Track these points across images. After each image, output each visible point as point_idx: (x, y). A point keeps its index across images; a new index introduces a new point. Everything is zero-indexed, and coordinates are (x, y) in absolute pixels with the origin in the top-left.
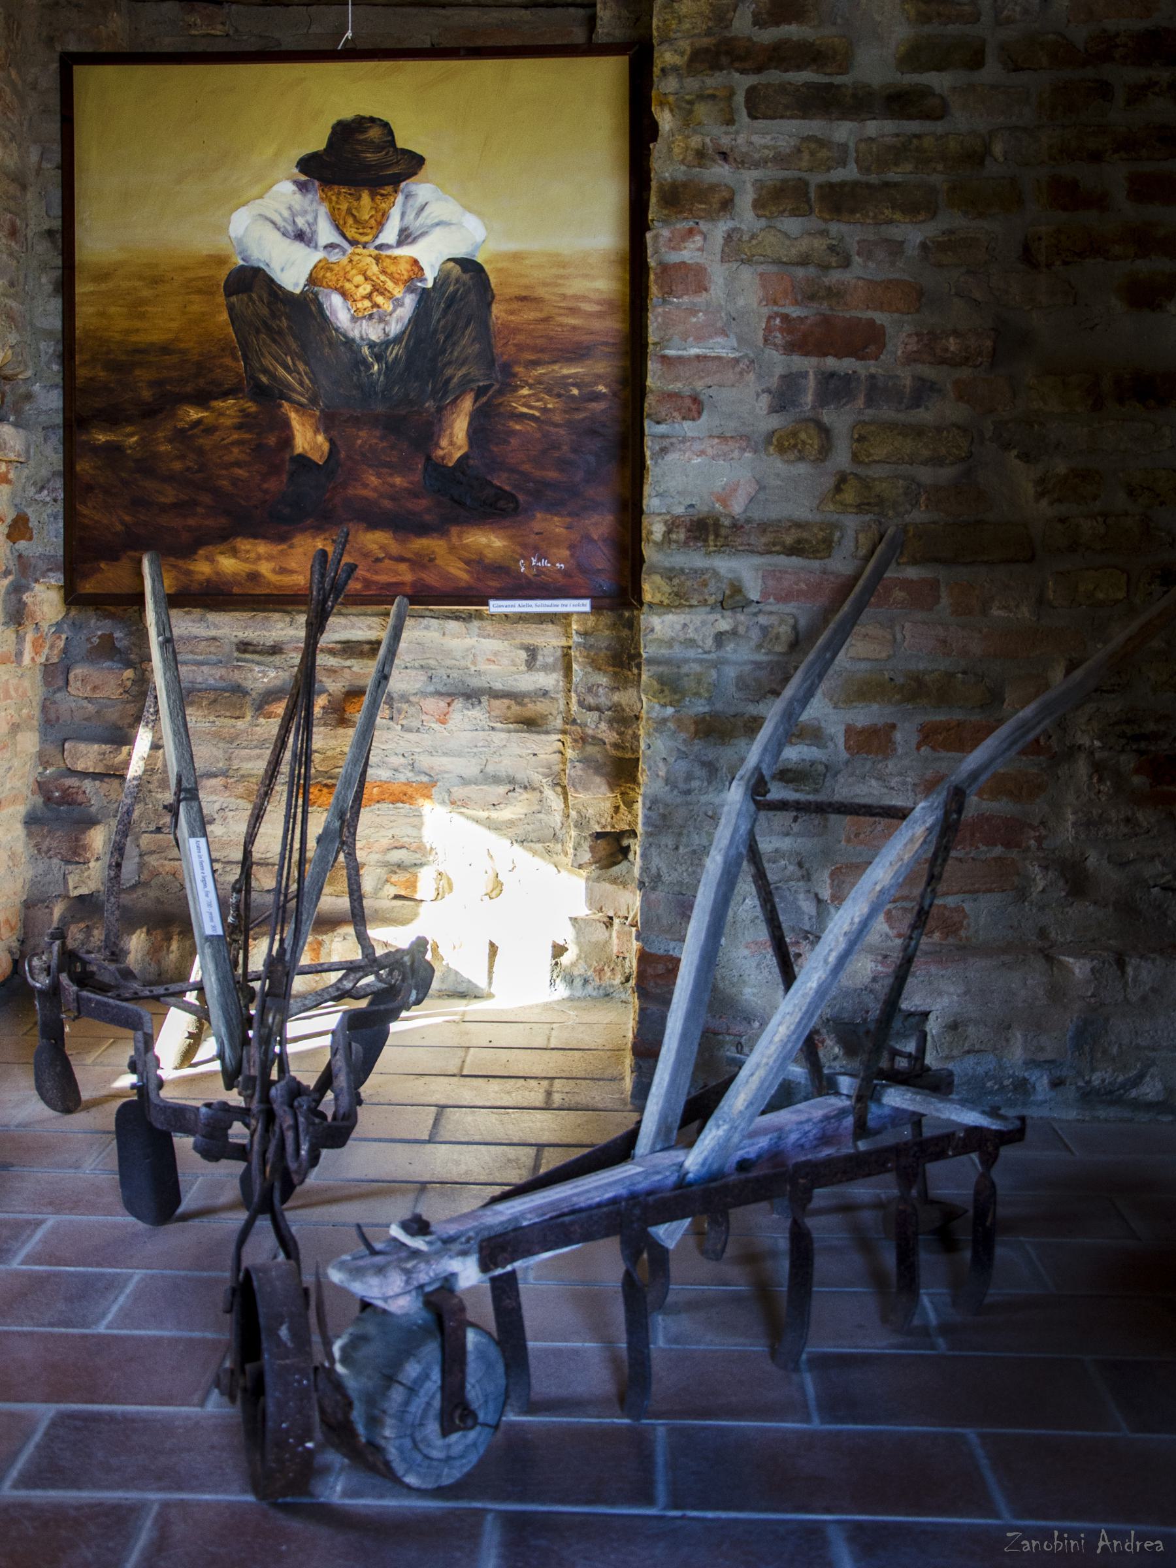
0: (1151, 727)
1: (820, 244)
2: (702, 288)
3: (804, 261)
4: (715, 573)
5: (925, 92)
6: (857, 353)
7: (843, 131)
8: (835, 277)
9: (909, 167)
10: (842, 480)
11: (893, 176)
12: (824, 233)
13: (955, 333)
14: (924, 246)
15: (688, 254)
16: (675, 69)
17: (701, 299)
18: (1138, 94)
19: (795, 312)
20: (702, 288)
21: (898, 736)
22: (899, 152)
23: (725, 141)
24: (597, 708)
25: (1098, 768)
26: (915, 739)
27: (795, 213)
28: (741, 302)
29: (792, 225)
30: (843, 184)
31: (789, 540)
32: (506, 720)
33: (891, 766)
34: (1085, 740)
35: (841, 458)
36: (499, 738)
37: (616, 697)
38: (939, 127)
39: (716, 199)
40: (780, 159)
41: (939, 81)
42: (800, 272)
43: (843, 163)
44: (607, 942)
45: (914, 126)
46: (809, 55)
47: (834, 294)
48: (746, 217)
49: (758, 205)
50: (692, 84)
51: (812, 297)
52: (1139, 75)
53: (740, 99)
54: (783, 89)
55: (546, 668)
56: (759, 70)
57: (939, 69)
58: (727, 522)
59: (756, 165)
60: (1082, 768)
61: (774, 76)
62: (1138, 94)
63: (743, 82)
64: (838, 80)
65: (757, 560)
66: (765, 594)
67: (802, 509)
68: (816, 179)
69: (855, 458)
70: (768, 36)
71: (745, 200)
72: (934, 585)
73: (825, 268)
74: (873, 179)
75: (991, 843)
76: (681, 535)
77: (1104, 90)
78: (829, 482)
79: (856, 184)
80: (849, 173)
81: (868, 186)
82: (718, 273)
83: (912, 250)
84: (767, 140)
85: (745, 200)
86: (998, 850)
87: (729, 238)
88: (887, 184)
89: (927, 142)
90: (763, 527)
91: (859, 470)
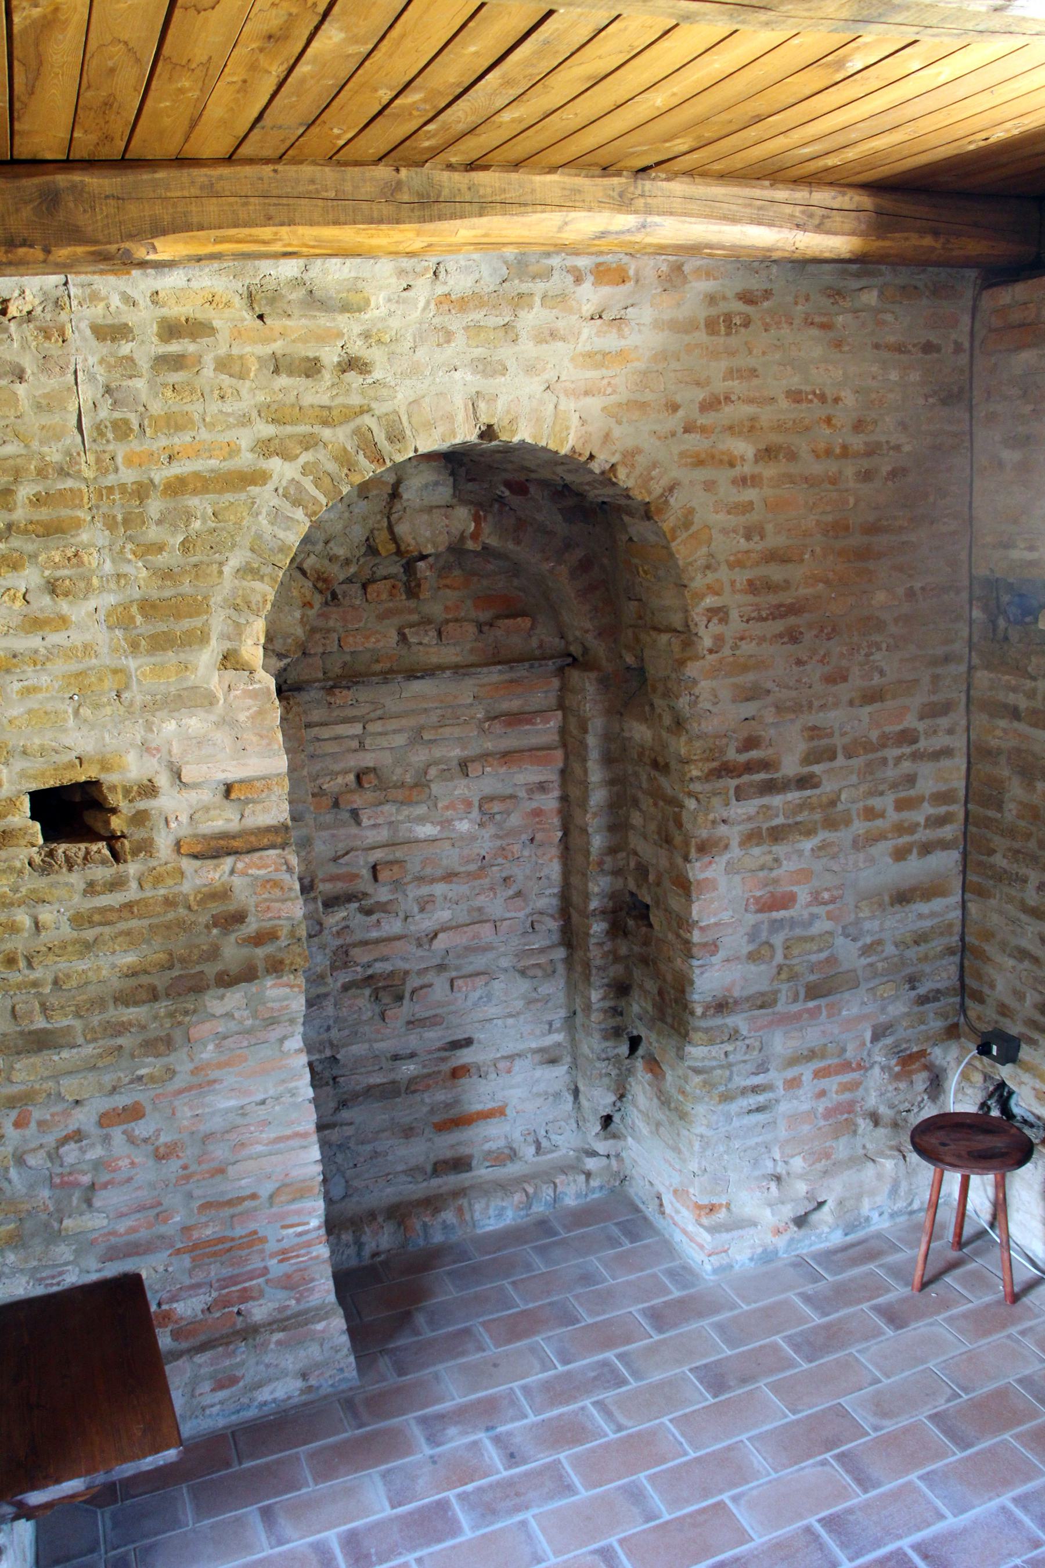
0: (904, 1046)
1: (769, 858)
2: (715, 889)
3: (762, 868)
4: (726, 1025)
5: (812, 776)
6: (785, 907)
7: (777, 800)
8: (775, 874)
9: (806, 813)
10: (780, 968)
11: (798, 819)
12: (770, 852)
13: (827, 890)
14: (812, 850)
15: (708, 874)
16: (698, 778)
17: (714, 894)
18: (898, 760)
19: (758, 894)
20: (715, 889)
21: (804, 1078)
22: (801, 807)
23: (725, 815)
24: (608, 1059)
25: (883, 1069)
26: (811, 1076)
27: (757, 845)
28: (734, 892)
29: (756, 851)
30: (777, 827)
31: (759, 1003)
32: (542, 1063)
33: (801, 1092)
34: (878, 1059)
35: (779, 958)
36: (538, 1073)
37: (616, 1051)
38: (817, 791)
39: (722, 844)
40: (750, 819)
41: (817, 769)
42: (761, 874)
43: (777, 816)
44: (609, 1165)
45: (808, 793)
46: (765, 765)
47: (776, 881)
48: (735, 851)
49: (742, 844)
50: (708, 787)
51: (766, 885)
52: (897, 752)
53: (732, 792)
54: (751, 784)
55: (557, 1031)
56: (739, 776)
57: (818, 763)
58: (731, 1001)
59: (739, 823)
60: (877, 1070)
61: (746, 778)
62: (898, 760)
63: (733, 783)
64: (775, 776)
65: (745, 1015)
66: (749, 1031)
67: (764, 986)
68: (765, 826)
69: (785, 957)
70: (743, 758)
71: (734, 843)
72: (819, 1007)
73: (771, 869)
74: (790, 821)
75: (842, 1114)
76: (712, 1011)
77: (884, 761)
78: (774, 971)
79: (783, 825)
80: (780, 820)
81: (789, 825)
82: (722, 882)
83: (807, 853)
84: (744, 811)
85: (734, 843)
86: (846, 1116)
87: (728, 863)
88: (797, 823)
89: (814, 800)
90: (748, 999)
91: (787, 962)
